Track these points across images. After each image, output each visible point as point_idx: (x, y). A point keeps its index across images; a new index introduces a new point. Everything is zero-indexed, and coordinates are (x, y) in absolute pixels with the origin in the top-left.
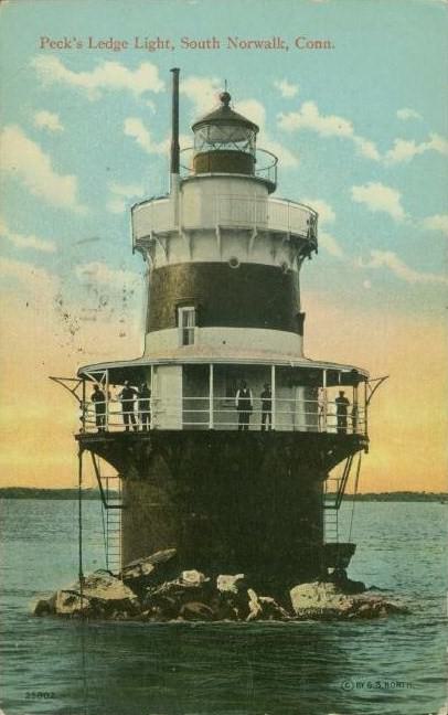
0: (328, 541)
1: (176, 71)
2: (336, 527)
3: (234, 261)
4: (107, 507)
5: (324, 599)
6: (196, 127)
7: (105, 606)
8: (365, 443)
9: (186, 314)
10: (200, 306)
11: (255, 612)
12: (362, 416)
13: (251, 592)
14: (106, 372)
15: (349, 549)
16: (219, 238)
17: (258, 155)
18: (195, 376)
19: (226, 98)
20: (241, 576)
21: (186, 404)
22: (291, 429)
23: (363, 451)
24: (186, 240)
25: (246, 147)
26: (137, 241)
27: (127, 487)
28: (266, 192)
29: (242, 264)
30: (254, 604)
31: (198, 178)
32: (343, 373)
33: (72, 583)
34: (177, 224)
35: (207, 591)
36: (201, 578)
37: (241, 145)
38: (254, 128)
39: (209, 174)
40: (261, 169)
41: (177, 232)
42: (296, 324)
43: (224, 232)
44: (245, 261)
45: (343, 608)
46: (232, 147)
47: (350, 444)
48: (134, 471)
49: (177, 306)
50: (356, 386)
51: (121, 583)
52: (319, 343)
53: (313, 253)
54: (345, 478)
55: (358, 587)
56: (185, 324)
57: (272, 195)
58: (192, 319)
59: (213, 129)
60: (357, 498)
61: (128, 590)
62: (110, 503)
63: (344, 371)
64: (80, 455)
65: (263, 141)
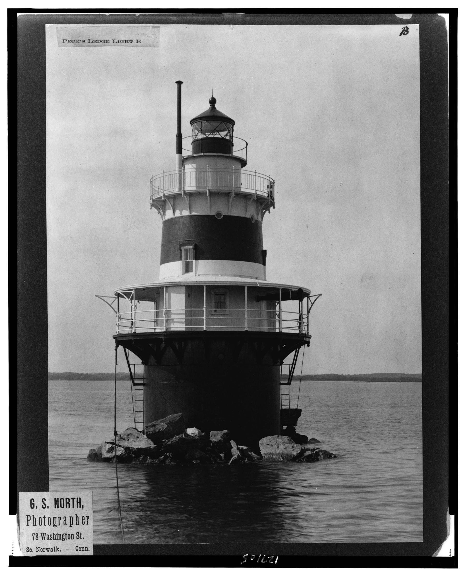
0: (284, 407)
1: (179, 83)
2: (289, 398)
3: (219, 214)
4: (135, 385)
5: (281, 447)
6: (193, 122)
7: (134, 453)
8: (307, 339)
9: (187, 251)
10: (196, 245)
11: (235, 457)
12: (305, 320)
13: (233, 443)
14: (133, 292)
15: (298, 412)
16: (209, 198)
17: (235, 141)
18: (193, 292)
19: (213, 101)
20: (226, 431)
21: (188, 313)
22: (258, 330)
23: (306, 345)
24: (187, 199)
25: (226, 135)
26: (153, 200)
27: (148, 371)
28: (240, 166)
29: (224, 216)
30: (235, 452)
31: (194, 157)
32: (292, 291)
33: (111, 437)
34: (180, 189)
35: (205, 429)
36: (199, 432)
37: (223, 133)
38: (232, 122)
39: (202, 154)
40: (236, 153)
41: (181, 194)
42: (261, 258)
43: (211, 193)
44: (226, 214)
45: (295, 453)
46: (217, 136)
47: (300, 340)
48: (152, 360)
49: (181, 245)
50: (301, 300)
51: (145, 437)
52: (275, 272)
53: (272, 208)
54: (294, 364)
55: (302, 440)
56: (186, 258)
57: (244, 168)
58: (191, 254)
59: (205, 123)
60: (301, 378)
61: (150, 441)
62: (136, 382)
63: (293, 290)
64: (116, 350)
65: (238, 131)
